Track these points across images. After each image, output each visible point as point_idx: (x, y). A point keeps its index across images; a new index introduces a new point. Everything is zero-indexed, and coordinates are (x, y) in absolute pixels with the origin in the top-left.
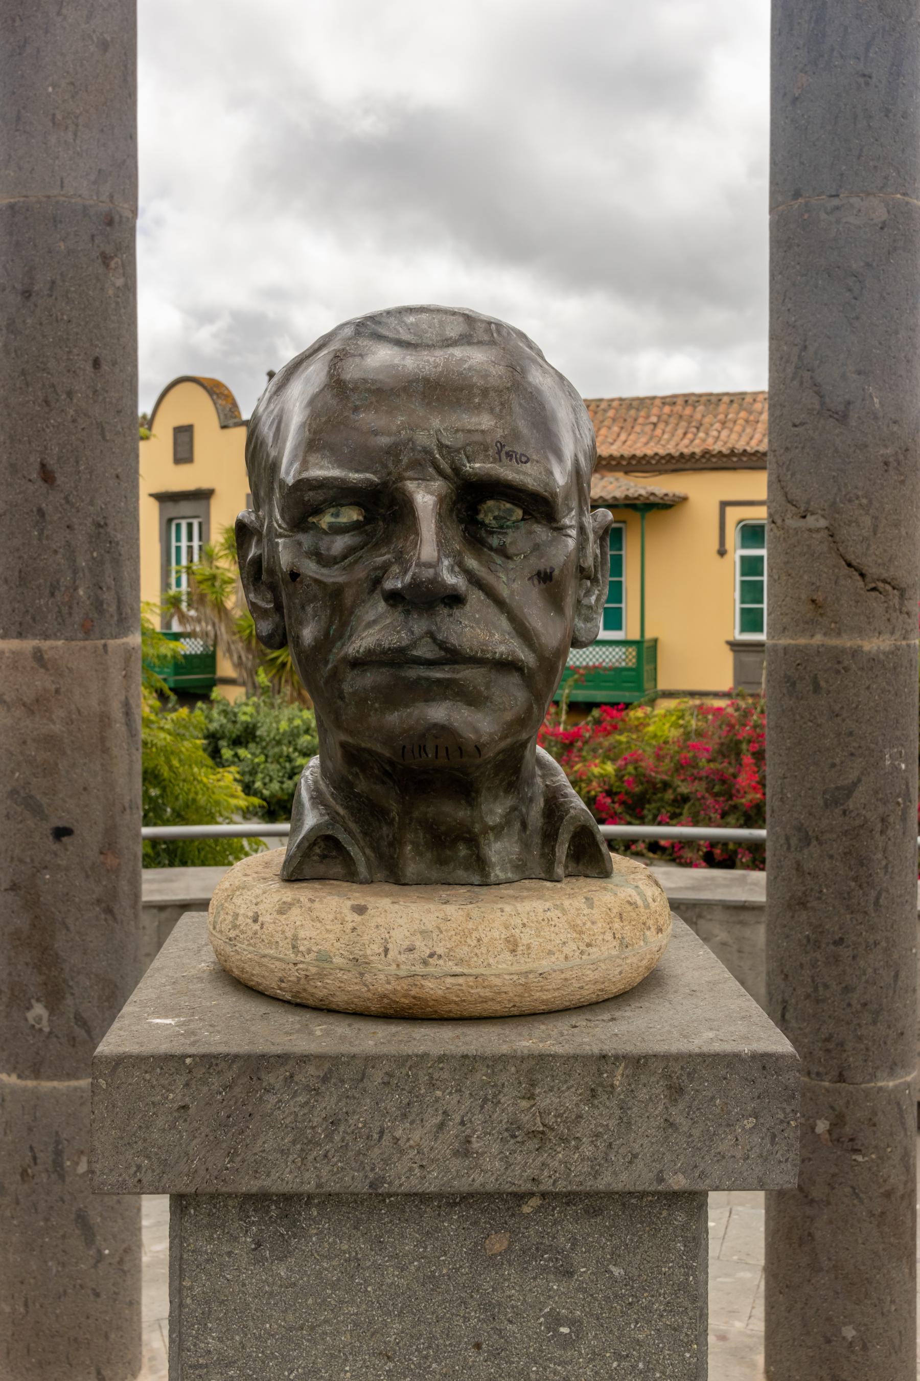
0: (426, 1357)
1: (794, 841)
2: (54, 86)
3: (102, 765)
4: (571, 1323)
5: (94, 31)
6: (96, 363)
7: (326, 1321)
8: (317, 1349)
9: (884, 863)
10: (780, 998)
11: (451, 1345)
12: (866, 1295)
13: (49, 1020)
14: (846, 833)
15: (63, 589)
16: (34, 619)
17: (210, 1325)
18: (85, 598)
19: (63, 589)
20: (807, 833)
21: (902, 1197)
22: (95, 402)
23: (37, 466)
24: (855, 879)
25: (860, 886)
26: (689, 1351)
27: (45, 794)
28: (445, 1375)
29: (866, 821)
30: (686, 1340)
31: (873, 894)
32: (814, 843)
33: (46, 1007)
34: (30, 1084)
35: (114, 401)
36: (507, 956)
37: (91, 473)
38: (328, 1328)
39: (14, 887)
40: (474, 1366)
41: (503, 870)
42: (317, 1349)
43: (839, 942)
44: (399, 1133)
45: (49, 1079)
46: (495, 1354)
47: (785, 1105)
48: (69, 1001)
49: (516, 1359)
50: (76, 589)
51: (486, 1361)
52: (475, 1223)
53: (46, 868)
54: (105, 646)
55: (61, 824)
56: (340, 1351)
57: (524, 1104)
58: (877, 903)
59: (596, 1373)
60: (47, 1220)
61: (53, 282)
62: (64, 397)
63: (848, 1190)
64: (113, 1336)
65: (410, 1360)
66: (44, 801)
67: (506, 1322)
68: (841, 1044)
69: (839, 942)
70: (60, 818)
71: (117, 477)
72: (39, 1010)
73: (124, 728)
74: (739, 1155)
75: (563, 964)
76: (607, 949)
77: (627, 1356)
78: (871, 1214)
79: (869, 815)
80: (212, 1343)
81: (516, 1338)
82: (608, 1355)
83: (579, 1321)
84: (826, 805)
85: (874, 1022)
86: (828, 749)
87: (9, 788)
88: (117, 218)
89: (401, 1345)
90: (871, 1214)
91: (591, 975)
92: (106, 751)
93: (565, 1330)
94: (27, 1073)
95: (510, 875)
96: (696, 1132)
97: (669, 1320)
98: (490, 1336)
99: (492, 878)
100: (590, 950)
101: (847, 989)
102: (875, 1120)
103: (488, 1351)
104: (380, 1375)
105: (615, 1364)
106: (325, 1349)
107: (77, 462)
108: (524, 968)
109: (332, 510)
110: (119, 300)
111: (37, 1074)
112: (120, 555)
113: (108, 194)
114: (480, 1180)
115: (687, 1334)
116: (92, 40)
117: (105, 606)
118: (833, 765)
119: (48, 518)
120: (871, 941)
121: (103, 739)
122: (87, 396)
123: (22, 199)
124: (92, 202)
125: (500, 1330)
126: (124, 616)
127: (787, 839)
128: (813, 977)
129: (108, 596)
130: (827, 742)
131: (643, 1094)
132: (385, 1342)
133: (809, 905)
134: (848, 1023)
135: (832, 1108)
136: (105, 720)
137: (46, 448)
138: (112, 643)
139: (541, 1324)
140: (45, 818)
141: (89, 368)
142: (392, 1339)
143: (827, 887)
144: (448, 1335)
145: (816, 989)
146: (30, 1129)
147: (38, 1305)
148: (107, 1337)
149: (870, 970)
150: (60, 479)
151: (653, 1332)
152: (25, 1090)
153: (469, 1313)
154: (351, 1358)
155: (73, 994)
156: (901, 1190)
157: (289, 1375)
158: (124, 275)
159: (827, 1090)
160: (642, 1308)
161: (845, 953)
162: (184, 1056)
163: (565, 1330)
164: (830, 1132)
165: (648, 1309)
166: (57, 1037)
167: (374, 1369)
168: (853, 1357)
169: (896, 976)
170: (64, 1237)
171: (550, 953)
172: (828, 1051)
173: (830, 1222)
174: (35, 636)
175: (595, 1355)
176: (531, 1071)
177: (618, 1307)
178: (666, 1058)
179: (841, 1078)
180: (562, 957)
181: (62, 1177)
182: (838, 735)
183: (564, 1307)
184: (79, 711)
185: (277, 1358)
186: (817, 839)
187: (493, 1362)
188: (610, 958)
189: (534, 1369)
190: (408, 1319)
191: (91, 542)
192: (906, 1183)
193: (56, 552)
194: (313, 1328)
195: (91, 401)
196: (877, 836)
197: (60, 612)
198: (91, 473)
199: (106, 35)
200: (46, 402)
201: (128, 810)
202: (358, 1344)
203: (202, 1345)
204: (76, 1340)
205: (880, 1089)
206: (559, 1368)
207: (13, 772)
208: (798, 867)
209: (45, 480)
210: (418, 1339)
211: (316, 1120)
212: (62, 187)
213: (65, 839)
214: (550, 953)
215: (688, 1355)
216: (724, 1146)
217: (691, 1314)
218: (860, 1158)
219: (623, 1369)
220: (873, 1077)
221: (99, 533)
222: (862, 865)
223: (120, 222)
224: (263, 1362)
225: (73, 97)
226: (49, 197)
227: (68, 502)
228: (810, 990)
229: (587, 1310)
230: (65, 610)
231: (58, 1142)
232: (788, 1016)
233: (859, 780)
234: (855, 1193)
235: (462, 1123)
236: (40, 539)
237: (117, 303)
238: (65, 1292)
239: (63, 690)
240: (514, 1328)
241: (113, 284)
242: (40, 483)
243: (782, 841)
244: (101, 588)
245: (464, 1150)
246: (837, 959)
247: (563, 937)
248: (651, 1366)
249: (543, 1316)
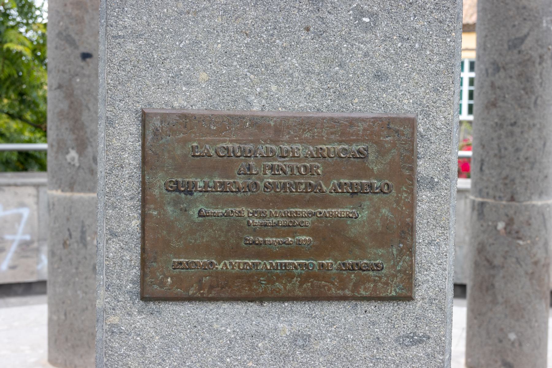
0: (272, 35)
1: (490, 71)
4: (371, 15)
7: (205, 8)
8: (198, 27)
9: (540, 81)
10: (479, 159)
11: (289, 27)
12: (523, 317)
13: (79, 160)
14: (520, 64)
17: (126, 9)
20: (498, 65)
21: (544, 266)
24: (524, 89)
25: (527, 93)
26: (449, 37)
27: (77, 34)
28: (285, 48)
29: (531, 57)
30: (447, 29)
31: (533, 98)
32: (502, 70)
33: (77, 152)
34: (68, 194)
38: (206, 14)
39: (60, 87)
40: (304, 42)
42: (198, 27)
43: (514, 124)
45: (79, 191)
46: (319, 35)
48: (90, 149)
49: (333, 39)
51: (312, 39)
53: (77, 75)
55: (85, 51)
56: (214, 29)
58: (535, 103)
59: (387, 50)
60: (77, 268)
63: (514, 260)
65: (261, 37)
66: (76, 38)
67: (327, 13)
68: (513, 180)
69: (514, 124)
70: (86, 48)
72: (73, 154)
77: (408, 39)
78: (526, 273)
79: (533, 53)
80: (128, 21)
81: (333, 24)
82: (395, 38)
83: (376, 14)
84: (509, 48)
85: (532, 168)
86: (511, 17)
87: (57, 31)
89: (255, 26)
90: (526, 273)
93: (366, 20)
94: (67, 188)
97: (436, 15)
98: (315, 22)
101: (517, 150)
102: (530, 222)
103: (314, 32)
104: (241, 47)
105: (399, 45)
106: (204, 28)
111: (72, 189)
115: (448, 25)
118: (514, 26)
120: (531, 123)
125: (323, 18)
127: (487, 70)
128: (498, 146)
130: (511, 13)
132: (244, 24)
133: (498, 105)
134: (517, 169)
135: (507, 215)
139: (350, 15)
140: (77, 47)
142: (250, 22)
143: (508, 94)
144: (287, 20)
145: (500, 151)
146: (68, 220)
147: (72, 315)
149: (530, 140)
151: (425, 23)
152: (65, 198)
153: (302, 6)
154: (221, 34)
155: (92, 146)
156: (543, 262)
157: (179, 45)
159: (505, 206)
160: (419, 7)
161: (517, 130)
163: (366, 20)
164: (505, 229)
166: (83, 169)
167: (237, 42)
168: (514, 350)
169: (544, 145)
170: (86, 278)
172: (506, 184)
173: (504, 277)
175: (386, 38)
177: (403, 5)
179: (512, 199)
181: (85, 245)
182: (518, 8)
183: (366, 4)
185: (171, 33)
186: (504, 68)
187: (317, 40)
189: (345, 46)
190: (261, 9)
192: (546, 258)
194: (196, 13)
196: (537, 65)
202: (226, 25)
203: (121, 23)
205: (533, 206)
206: (362, 46)
207: (59, 22)
208: (493, 85)
210: (267, 23)
215: (449, 40)
217: (452, 12)
218: (521, 242)
219: (405, 47)
220: (530, 198)
222: (528, 81)
224: (162, 35)
228: (496, 152)
229: (382, 6)
231: (83, 227)
232: (484, 168)
233: (528, 34)
234: (518, 261)
238: (87, 308)
240: (332, 17)
243: (484, 72)
246: (512, 134)
248: (423, 46)
249: (352, 9)
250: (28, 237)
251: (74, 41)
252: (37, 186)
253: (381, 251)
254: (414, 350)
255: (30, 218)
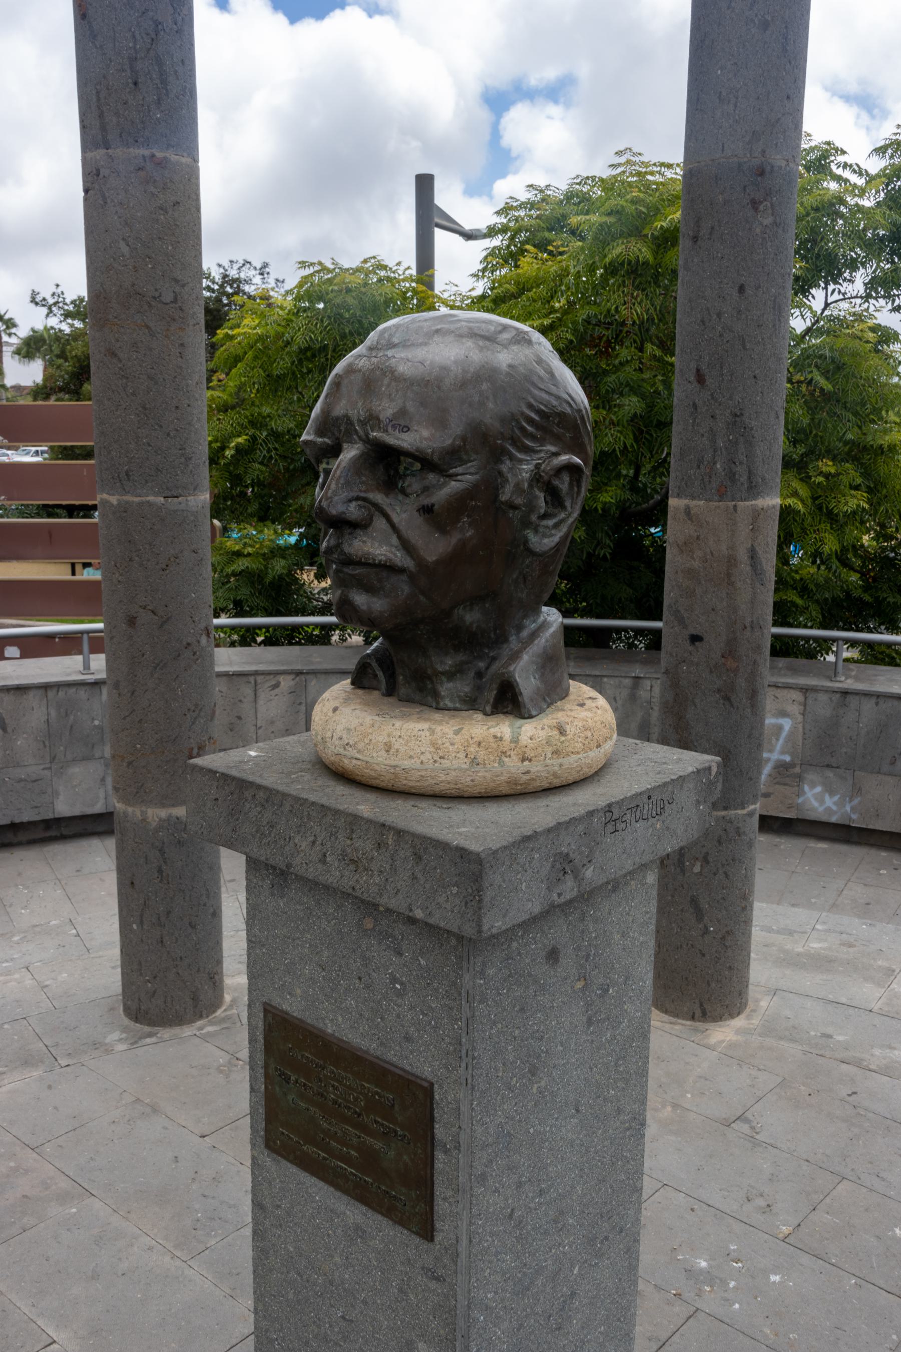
2: (721, 68)
3: (727, 594)
4: (402, 984)
5: (756, 16)
6: (741, 289)
15: (706, 463)
16: (686, 484)
18: (721, 470)
19: (706, 463)
22: (738, 319)
23: (694, 371)
35: (755, 318)
36: (383, 753)
37: (731, 375)
41: (452, 701)
44: (296, 841)
47: (472, 884)
50: (715, 463)
52: (359, 908)
54: (735, 506)
55: (695, 633)
57: (349, 842)
60: (673, 896)
61: (713, 228)
62: (715, 317)
64: (713, 985)
66: (686, 615)
71: (755, 377)
73: (748, 568)
74: (449, 908)
75: (418, 766)
76: (462, 762)
88: (768, 169)
91: (443, 777)
92: (731, 584)
95: (458, 705)
96: (428, 886)
99: (441, 704)
100: (443, 761)
107: (722, 368)
108: (393, 763)
109: (325, 460)
110: (766, 236)
112: (753, 437)
113: (760, 150)
114: (330, 880)
116: (755, 23)
117: (737, 476)
119: (699, 410)
121: (729, 575)
122: (732, 316)
123: (696, 165)
124: (746, 159)
126: (754, 483)
129: (741, 470)
131: (402, 854)
136: (732, 562)
137: (701, 357)
138: (741, 504)
140: (685, 627)
141: (735, 294)
148: (709, 984)
150: (709, 381)
158: (773, 215)
162: (216, 772)
163: (398, 986)
165: (436, 990)
170: (682, 910)
171: (411, 757)
174: (686, 497)
176: (351, 823)
178: (414, 835)
180: (419, 762)
181: (683, 871)
184: (712, 553)
188: (460, 769)
191: (728, 429)
193: (703, 435)
195: (735, 319)
197: (703, 480)
198: (731, 375)
199: (766, 17)
200: (703, 322)
201: (749, 629)
204: (686, 978)
209: (699, 382)
211: (265, 823)
212: (723, 150)
213: (697, 643)
214: (411, 757)
216: (441, 900)
221: (736, 421)
223: (772, 171)
225: (735, 75)
226: (713, 160)
227: (713, 398)
230: (707, 479)
235: (322, 844)
236: (693, 426)
237: (764, 239)
239: (702, 537)
241: (761, 224)
242: (695, 383)
244: (734, 463)
245: (323, 860)
247: (423, 749)
250: (788, 758)
251: (683, 618)
252: (805, 690)
253: (404, 1190)
254: (433, 1285)
255: (791, 733)
